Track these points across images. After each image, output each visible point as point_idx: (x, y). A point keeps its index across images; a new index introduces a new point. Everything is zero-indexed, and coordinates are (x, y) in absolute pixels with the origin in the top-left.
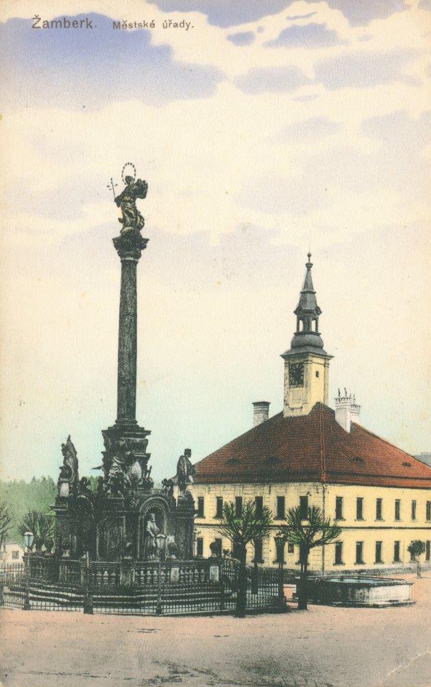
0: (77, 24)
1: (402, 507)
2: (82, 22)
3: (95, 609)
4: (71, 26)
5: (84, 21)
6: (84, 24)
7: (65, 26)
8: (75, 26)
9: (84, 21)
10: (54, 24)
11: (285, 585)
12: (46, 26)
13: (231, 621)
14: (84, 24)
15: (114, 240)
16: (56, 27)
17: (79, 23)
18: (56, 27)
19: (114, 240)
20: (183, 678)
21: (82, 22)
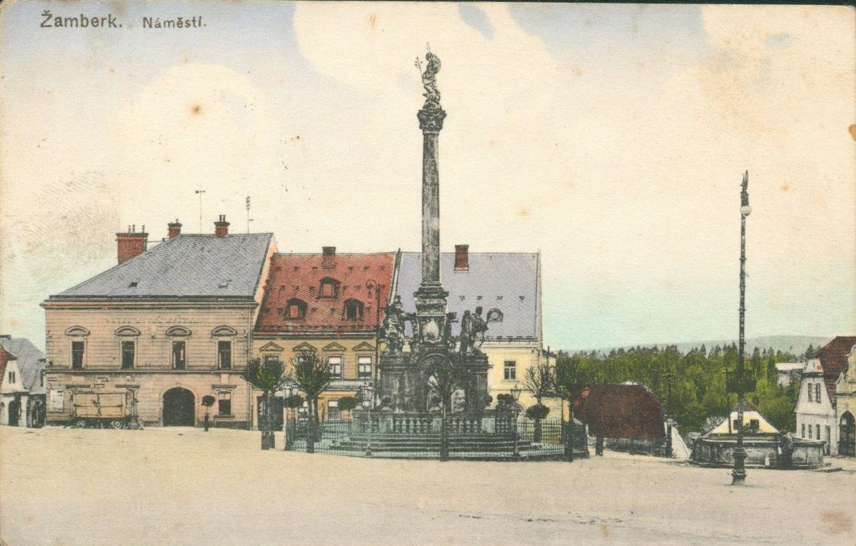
0: (97, 22)
1: (821, 428)
2: (103, 19)
3: (182, 359)
4: (90, 24)
5: (105, 19)
6: (106, 22)
7: (82, 25)
8: (95, 24)
9: (105, 19)
10: (69, 22)
11: (566, 403)
12: (58, 24)
13: (814, 410)
14: (106, 22)
15: (335, 248)
16: (71, 26)
17: (100, 21)
18: (71, 26)
19: (335, 248)
20: (109, 379)
21: (103, 19)
